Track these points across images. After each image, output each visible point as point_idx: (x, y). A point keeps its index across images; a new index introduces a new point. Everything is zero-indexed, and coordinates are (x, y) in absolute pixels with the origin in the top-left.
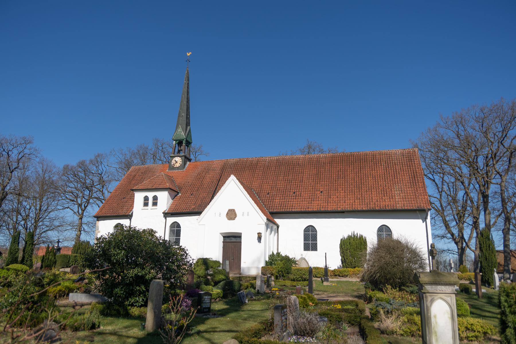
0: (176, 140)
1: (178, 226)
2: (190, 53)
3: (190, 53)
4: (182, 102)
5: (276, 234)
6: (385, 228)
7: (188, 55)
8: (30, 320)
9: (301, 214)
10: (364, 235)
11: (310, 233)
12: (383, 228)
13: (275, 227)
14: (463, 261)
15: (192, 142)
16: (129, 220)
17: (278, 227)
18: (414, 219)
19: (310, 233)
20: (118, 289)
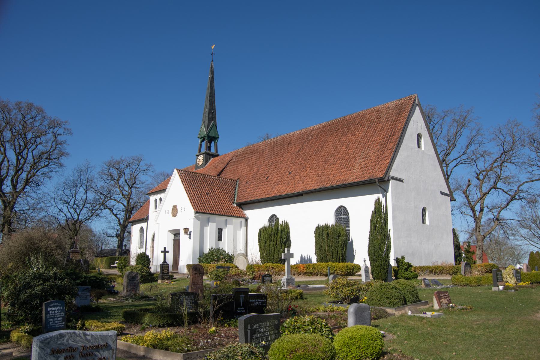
0: (201, 138)
1: (346, 212)
2: (214, 45)
3: (214, 45)
4: (207, 98)
5: (243, 228)
6: (344, 209)
7: (213, 48)
8: (286, 291)
9: (265, 202)
10: (260, 227)
11: (343, 216)
12: (342, 210)
13: (243, 220)
14: (151, 282)
15: (218, 138)
16: (146, 223)
17: (247, 220)
18: (373, 194)
19: (343, 216)
20: (7, 309)
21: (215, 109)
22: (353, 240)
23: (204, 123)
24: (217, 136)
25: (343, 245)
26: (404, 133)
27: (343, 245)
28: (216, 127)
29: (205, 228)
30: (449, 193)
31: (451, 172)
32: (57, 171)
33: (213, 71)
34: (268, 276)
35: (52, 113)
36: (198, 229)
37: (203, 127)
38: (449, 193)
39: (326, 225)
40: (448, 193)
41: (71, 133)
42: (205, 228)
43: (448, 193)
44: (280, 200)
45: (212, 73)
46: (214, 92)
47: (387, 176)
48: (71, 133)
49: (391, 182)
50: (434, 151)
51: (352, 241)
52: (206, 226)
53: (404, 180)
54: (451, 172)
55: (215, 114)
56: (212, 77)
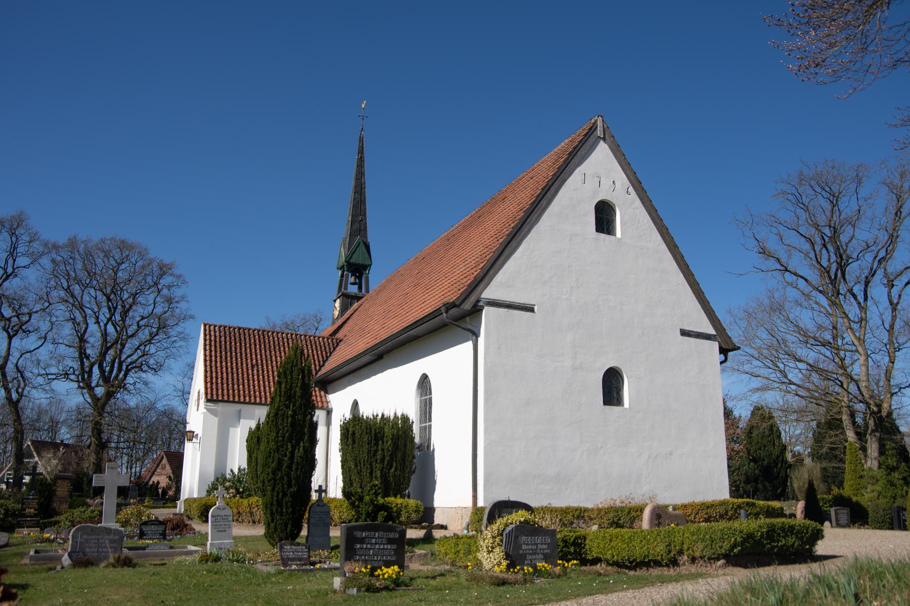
7: (363, 106)
15: (370, 265)
21: (365, 215)
22: (435, 448)
23: (344, 244)
24: (367, 263)
25: (387, 459)
26: (544, 202)
27: (387, 459)
28: (367, 247)
29: (231, 429)
30: (714, 333)
31: (900, 296)
32: (180, 347)
33: (363, 148)
34: (155, 524)
35: (159, 252)
36: (214, 432)
37: (342, 249)
38: (714, 333)
39: (403, 415)
40: (712, 331)
41: (184, 282)
42: (231, 429)
43: (712, 331)
44: (362, 369)
45: (361, 151)
46: (364, 183)
47: (472, 299)
48: (184, 282)
49: (488, 314)
50: (659, 238)
51: (434, 449)
52: (234, 426)
53: (536, 308)
54: (900, 296)
55: (366, 223)
56: (361, 157)
